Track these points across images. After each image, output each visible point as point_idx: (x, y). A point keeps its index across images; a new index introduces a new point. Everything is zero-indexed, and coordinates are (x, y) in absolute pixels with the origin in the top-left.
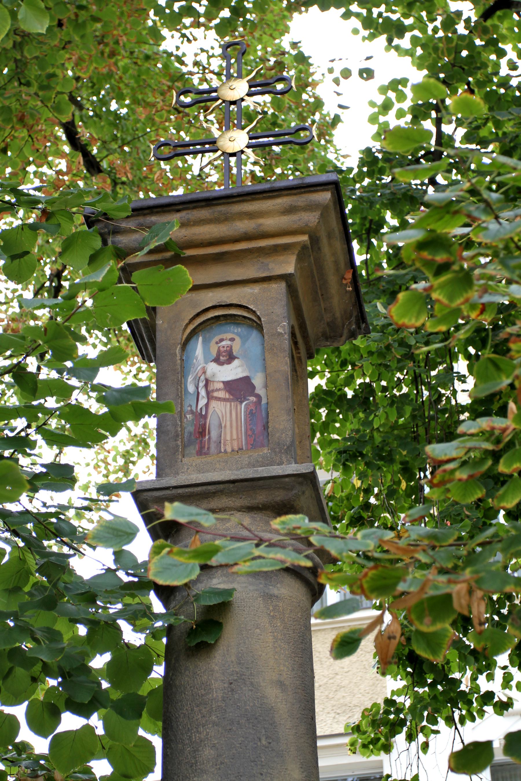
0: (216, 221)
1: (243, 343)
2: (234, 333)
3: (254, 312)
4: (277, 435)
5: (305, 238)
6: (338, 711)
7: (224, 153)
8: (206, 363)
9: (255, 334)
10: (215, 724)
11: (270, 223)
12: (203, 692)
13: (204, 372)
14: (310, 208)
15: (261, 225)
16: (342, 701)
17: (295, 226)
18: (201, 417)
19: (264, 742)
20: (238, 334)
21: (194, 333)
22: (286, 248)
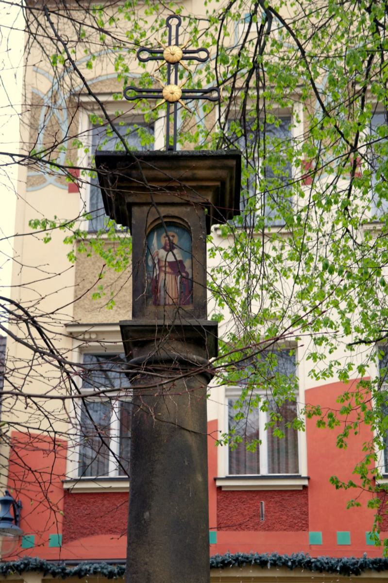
0: (170, 168)
1: (179, 240)
2: (174, 232)
3: (187, 223)
4: (198, 299)
5: (218, 184)
6: (120, 306)
7: (167, 101)
8: (159, 249)
9: (186, 235)
10: (163, 453)
11: (201, 173)
12: (157, 436)
13: (158, 255)
14: (223, 168)
15: (195, 174)
16: (123, 298)
17: (214, 177)
18: (156, 281)
19: (186, 463)
20: (176, 233)
21: (152, 231)
22: (207, 188)
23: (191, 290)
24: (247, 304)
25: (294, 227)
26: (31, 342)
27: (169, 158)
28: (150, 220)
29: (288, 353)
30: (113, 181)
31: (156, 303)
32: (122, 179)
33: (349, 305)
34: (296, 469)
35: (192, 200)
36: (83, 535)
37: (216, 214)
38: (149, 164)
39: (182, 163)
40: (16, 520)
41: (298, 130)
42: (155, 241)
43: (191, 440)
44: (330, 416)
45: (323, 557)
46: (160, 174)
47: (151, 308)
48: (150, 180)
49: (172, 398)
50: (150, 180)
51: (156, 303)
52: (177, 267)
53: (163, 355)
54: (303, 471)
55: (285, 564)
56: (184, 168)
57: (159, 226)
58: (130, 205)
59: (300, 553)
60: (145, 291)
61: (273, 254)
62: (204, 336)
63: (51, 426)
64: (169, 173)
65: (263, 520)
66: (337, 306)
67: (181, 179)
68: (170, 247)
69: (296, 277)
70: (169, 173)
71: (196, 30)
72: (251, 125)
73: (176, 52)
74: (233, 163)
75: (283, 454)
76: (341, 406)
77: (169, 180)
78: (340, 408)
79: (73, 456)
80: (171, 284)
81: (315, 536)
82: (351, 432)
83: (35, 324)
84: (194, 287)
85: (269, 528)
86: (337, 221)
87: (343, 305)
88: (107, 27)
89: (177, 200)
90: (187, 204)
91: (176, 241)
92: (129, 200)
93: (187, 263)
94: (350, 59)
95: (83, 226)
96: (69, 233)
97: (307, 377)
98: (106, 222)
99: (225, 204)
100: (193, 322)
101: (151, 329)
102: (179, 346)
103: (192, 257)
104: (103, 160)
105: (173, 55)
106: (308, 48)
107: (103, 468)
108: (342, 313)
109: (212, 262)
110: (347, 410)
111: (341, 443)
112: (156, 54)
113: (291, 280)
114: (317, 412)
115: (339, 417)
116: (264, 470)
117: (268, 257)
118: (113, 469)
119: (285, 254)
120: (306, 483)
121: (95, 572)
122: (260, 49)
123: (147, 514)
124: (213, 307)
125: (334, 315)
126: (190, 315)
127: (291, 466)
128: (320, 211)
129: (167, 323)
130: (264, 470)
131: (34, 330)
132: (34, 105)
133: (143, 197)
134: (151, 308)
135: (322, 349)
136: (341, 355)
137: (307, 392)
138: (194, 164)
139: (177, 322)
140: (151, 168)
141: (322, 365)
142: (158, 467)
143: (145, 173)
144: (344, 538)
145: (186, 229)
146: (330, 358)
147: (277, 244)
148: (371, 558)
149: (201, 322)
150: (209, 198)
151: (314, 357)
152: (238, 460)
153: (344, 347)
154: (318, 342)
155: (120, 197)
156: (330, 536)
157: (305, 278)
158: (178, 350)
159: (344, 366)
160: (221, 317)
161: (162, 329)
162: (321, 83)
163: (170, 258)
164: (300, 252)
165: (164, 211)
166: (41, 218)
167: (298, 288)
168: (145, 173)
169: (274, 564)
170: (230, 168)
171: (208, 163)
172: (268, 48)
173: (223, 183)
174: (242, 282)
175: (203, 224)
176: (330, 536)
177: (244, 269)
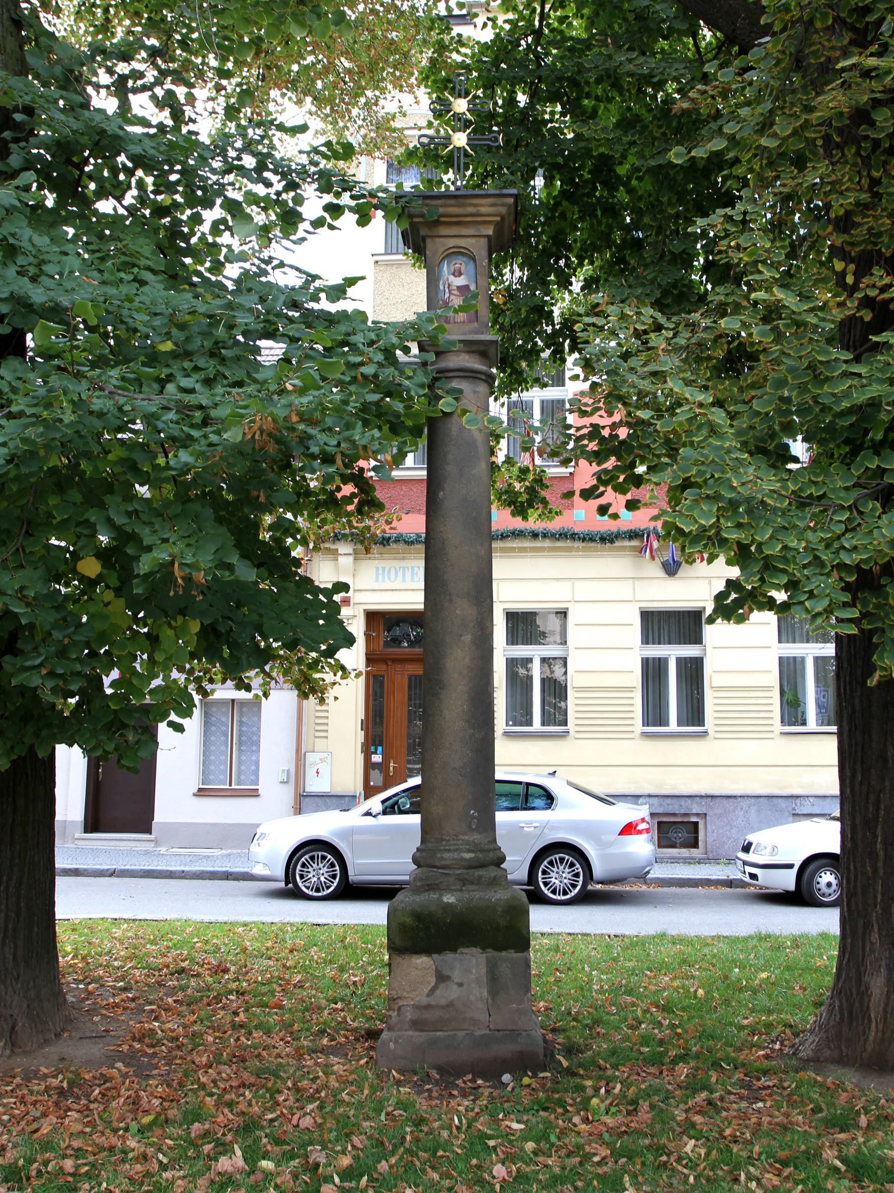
5: (499, 219)
11: (483, 210)
14: (503, 205)
57: (450, 254)
68: (458, 273)
123: (441, 494)
142: (450, 457)
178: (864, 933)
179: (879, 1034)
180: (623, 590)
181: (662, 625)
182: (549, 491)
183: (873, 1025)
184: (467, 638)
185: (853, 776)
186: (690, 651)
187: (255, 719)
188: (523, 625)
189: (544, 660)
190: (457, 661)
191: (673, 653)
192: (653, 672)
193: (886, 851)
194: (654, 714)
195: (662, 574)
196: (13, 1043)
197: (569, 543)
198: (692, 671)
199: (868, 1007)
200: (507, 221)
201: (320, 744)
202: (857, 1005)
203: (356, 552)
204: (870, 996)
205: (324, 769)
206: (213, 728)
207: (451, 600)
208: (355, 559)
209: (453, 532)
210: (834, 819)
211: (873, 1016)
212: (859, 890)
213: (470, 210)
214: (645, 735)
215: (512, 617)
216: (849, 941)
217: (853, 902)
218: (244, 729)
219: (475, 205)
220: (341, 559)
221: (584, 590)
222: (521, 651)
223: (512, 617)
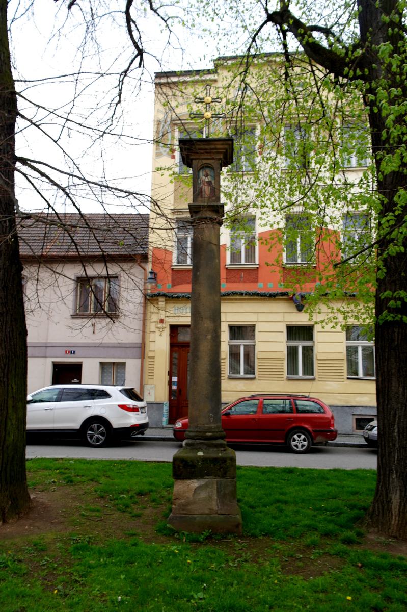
5: (224, 151)
11: (218, 147)
14: (227, 144)
18: (201, 189)
21: (200, 169)
22: (221, 153)
23: (214, 191)
24: (236, 200)
25: (255, 172)
26: (155, 211)
27: (207, 141)
28: (199, 165)
29: (253, 219)
30: (185, 150)
31: (202, 197)
32: (188, 149)
33: (275, 199)
34: (254, 261)
35: (215, 157)
36: (179, 284)
37: (224, 163)
38: (199, 143)
39: (211, 143)
40: (155, 279)
41: (258, 132)
42: (201, 173)
43: (214, 247)
44: (266, 240)
45: (263, 292)
46: (203, 147)
47: (200, 199)
48: (200, 149)
49: (207, 231)
50: (200, 149)
51: (202, 197)
52: (209, 183)
53: (204, 216)
54: (257, 262)
55: (250, 294)
56: (212, 144)
57: (203, 167)
58: (192, 159)
59: (255, 291)
60: (197, 193)
61: (247, 181)
62: (219, 209)
63: (64, 127)
64: (207, 147)
65: (242, 279)
66: (270, 199)
67: (211, 149)
68: (207, 176)
69: (255, 189)
70: (207, 147)
71: (218, 92)
72: (241, 131)
73: (209, 99)
74: (230, 142)
75: (250, 257)
76: (270, 237)
77: (206, 149)
78: (270, 239)
79: (175, 256)
80: (207, 190)
81: (260, 285)
82: (273, 247)
83: (157, 204)
84: (216, 190)
85: (244, 282)
86: (271, 168)
87: (272, 200)
88: (183, 91)
89: (209, 157)
90: (213, 159)
91: (209, 173)
92: (191, 157)
93: (213, 182)
94: (277, 102)
95: (177, 170)
96: (171, 172)
97: (259, 229)
98: (185, 167)
99: (228, 159)
100: (215, 204)
101: (199, 206)
102: (210, 213)
103: (215, 179)
104: (182, 142)
105: (379, 269)
106: (261, 100)
107: (185, 261)
108: (272, 203)
109: (222, 183)
110: (273, 238)
111: (269, 250)
112: (201, 100)
113: (253, 190)
114: (261, 239)
115: (269, 240)
116: (243, 262)
117: (245, 182)
118: (189, 262)
119: (251, 181)
120: (258, 266)
121: (183, 297)
122: (243, 98)
123: (198, 273)
124: (223, 199)
125: (268, 203)
126: (214, 201)
127: (253, 261)
128: (265, 164)
129: (206, 204)
130: (243, 262)
131: (157, 207)
132: (159, 123)
133: (197, 157)
134: (200, 199)
135: (264, 217)
136: (272, 219)
137: (259, 234)
138: (215, 143)
139: (209, 204)
140: (199, 145)
141: (263, 222)
142: (202, 257)
143: (197, 147)
144: (270, 285)
145: (212, 168)
146: (267, 219)
147: (249, 177)
148: (280, 292)
149: (218, 204)
150: (221, 156)
151: (261, 219)
152: (234, 259)
153: (272, 215)
154: (263, 214)
155: (188, 156)
156: (265, 285)
157: (258, 189)
158: (209, 214)
159: (272, 222)
160: (226, 204)
161: (204, 207)
162: (266, 113)
163: (207, 180)
164: (257, 179)
165: (204, 161)
166: (160, 167)
167: (256, 194)
168: (197, 147)
169: (246, 294)
170: (229, 144)
171: (221, 143)
172: (245, 99)
173: (227, 151)
174: (235, 191)
175: (219, 166)
176: (265, 285)
177: (235, 186)
178: (389, 474)
179: (397, 522)
180: (279, 317)
181: (294, 332)
182: (295, 6)
183: (394, 517)
184: (209, 337)
185: (384, 402)
186: (307, 343)
187: (123, 371)
188: (237, 331)
189: (245, 346)
190: (205, 347)
191: (300, 344)
192: (292, 352)
193: (399, 436)
194: (292, 369)
195: (295, 310)
196: (4, 522)
197: (256, 297)
198: (308, 351)
199: (391, 508)
200: (229, 151)
201: (150, 381)
202: (386, 507)
203: (166, 300)
204: (392, 503)
205: (152, 392)
206: (105, 375)
207: (202, 320)
208: (166, 303)
209: (203, 290)
210: (24, 161)
211: (393, 513)
212: (387, 454)
213: (213, 147)
214: (289, 379)
215: (232, 328)
216: (382, 477)
217: (384, 460)
218: (119, 375)
219: (215, 145)
220: (160, 303)
221: (262, 317)
222: (236, 342)
223: (232, 328)
